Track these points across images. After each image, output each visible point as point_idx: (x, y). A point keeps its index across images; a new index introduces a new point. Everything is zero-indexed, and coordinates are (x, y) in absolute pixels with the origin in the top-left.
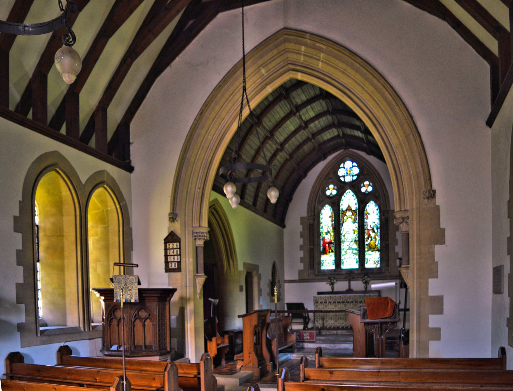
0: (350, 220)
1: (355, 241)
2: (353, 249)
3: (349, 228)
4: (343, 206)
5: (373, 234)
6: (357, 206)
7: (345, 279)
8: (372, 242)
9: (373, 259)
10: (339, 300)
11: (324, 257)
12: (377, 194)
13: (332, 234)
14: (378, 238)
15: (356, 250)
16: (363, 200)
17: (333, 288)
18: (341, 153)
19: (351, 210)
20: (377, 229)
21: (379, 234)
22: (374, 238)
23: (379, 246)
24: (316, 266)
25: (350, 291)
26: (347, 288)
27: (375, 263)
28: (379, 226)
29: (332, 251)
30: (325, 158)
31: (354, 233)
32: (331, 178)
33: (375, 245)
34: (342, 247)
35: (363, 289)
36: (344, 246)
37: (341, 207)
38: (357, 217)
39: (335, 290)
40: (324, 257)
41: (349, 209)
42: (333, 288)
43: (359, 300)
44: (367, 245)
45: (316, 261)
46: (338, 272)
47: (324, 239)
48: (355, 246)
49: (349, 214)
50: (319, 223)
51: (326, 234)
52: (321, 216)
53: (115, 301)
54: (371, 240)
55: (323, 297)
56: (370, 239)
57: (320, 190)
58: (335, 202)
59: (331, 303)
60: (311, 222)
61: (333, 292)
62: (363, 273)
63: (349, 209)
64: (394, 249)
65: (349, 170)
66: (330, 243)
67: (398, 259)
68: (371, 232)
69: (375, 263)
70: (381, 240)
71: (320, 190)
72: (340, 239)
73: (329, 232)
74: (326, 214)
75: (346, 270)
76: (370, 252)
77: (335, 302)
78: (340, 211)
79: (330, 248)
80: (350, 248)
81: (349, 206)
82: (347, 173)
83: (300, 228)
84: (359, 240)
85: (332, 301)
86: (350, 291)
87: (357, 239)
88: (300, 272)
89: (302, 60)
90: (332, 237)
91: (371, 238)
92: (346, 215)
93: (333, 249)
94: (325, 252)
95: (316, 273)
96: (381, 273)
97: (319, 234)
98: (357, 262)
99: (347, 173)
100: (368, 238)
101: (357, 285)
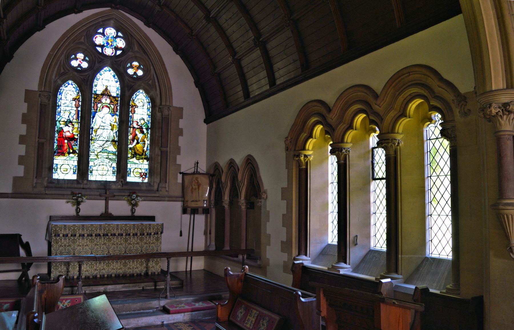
0: (106, 110)
1: (113, 141)
2: (109, 153)
3: (104, 121)
4: (99, 87)
5: (140, 136)
6: (119, 92)
7: (100, 197)
8: (137, 146)
9: (138, 170)
10: (98, 232)
11: (58, 160)
12: (150, 82)
13: (76, 125)
14: (147, 142)
15: (114, 154)
16: (129, 86)
17: (78, 210)
18: (97, 14)
19: (109, 96)
21: (149, 135)
22: (143, 141)
23: (148, 153)
24: (45, 173)
25: (106, 216)
26: (103, 210)
27: (141, 176)
28: (150, 125)
29: (74, 152)
30: (80, 11)
31: (112, 130)
32: (81, 43)
33: (143, 150)
34: (92, 148)
35: (129, 213)
36: (95, 146)
37: (94, 89)
38: (118, 108)
39: (137, 214)
40: (58, 160)
41: (106, 93)
42: (78, 210)
43: (132, 232)
44: (130, 148)
46: (81, 186)
47: (61, 131)
48: (112, 148)
49: (106, 101)
50: (55, 106)
52: (59, 97)
53: (430, 113)
54: (138, 143)
55: (70, 227)
56: (136, 141)
57: (63, 56)
58: (85, 81)
59: (84, 235)
61: (133, 218)
62: (121, 188)
63: (106, 93)
64: (175, 160)
65: (109, 40)
66: (72, 138)
67: (180, 173)
68: (137, 132)
69: (141, 176)
71: (63, 56)
72: (89, 134)
73: (71, 122)
74: (68, 94)
75: (96, 182)
76: (134, 160)
77: (91, 235)
78: (92, 94)
79: (70, 147)
80: (103, 151)
81: (106, 89)
82: (108, 43)
83: (24, 108)
85: (86, 233)
86: (106, 216)
87: (116, 139)
88: (16, 180)
90: (75, 130)
91: (138, 141)
92: (100, 102)
93: (76, 148)
96: (149, 191)
97: (54, 122)
98: (113, 173)
99: (108, 43)
101: (119, 207)
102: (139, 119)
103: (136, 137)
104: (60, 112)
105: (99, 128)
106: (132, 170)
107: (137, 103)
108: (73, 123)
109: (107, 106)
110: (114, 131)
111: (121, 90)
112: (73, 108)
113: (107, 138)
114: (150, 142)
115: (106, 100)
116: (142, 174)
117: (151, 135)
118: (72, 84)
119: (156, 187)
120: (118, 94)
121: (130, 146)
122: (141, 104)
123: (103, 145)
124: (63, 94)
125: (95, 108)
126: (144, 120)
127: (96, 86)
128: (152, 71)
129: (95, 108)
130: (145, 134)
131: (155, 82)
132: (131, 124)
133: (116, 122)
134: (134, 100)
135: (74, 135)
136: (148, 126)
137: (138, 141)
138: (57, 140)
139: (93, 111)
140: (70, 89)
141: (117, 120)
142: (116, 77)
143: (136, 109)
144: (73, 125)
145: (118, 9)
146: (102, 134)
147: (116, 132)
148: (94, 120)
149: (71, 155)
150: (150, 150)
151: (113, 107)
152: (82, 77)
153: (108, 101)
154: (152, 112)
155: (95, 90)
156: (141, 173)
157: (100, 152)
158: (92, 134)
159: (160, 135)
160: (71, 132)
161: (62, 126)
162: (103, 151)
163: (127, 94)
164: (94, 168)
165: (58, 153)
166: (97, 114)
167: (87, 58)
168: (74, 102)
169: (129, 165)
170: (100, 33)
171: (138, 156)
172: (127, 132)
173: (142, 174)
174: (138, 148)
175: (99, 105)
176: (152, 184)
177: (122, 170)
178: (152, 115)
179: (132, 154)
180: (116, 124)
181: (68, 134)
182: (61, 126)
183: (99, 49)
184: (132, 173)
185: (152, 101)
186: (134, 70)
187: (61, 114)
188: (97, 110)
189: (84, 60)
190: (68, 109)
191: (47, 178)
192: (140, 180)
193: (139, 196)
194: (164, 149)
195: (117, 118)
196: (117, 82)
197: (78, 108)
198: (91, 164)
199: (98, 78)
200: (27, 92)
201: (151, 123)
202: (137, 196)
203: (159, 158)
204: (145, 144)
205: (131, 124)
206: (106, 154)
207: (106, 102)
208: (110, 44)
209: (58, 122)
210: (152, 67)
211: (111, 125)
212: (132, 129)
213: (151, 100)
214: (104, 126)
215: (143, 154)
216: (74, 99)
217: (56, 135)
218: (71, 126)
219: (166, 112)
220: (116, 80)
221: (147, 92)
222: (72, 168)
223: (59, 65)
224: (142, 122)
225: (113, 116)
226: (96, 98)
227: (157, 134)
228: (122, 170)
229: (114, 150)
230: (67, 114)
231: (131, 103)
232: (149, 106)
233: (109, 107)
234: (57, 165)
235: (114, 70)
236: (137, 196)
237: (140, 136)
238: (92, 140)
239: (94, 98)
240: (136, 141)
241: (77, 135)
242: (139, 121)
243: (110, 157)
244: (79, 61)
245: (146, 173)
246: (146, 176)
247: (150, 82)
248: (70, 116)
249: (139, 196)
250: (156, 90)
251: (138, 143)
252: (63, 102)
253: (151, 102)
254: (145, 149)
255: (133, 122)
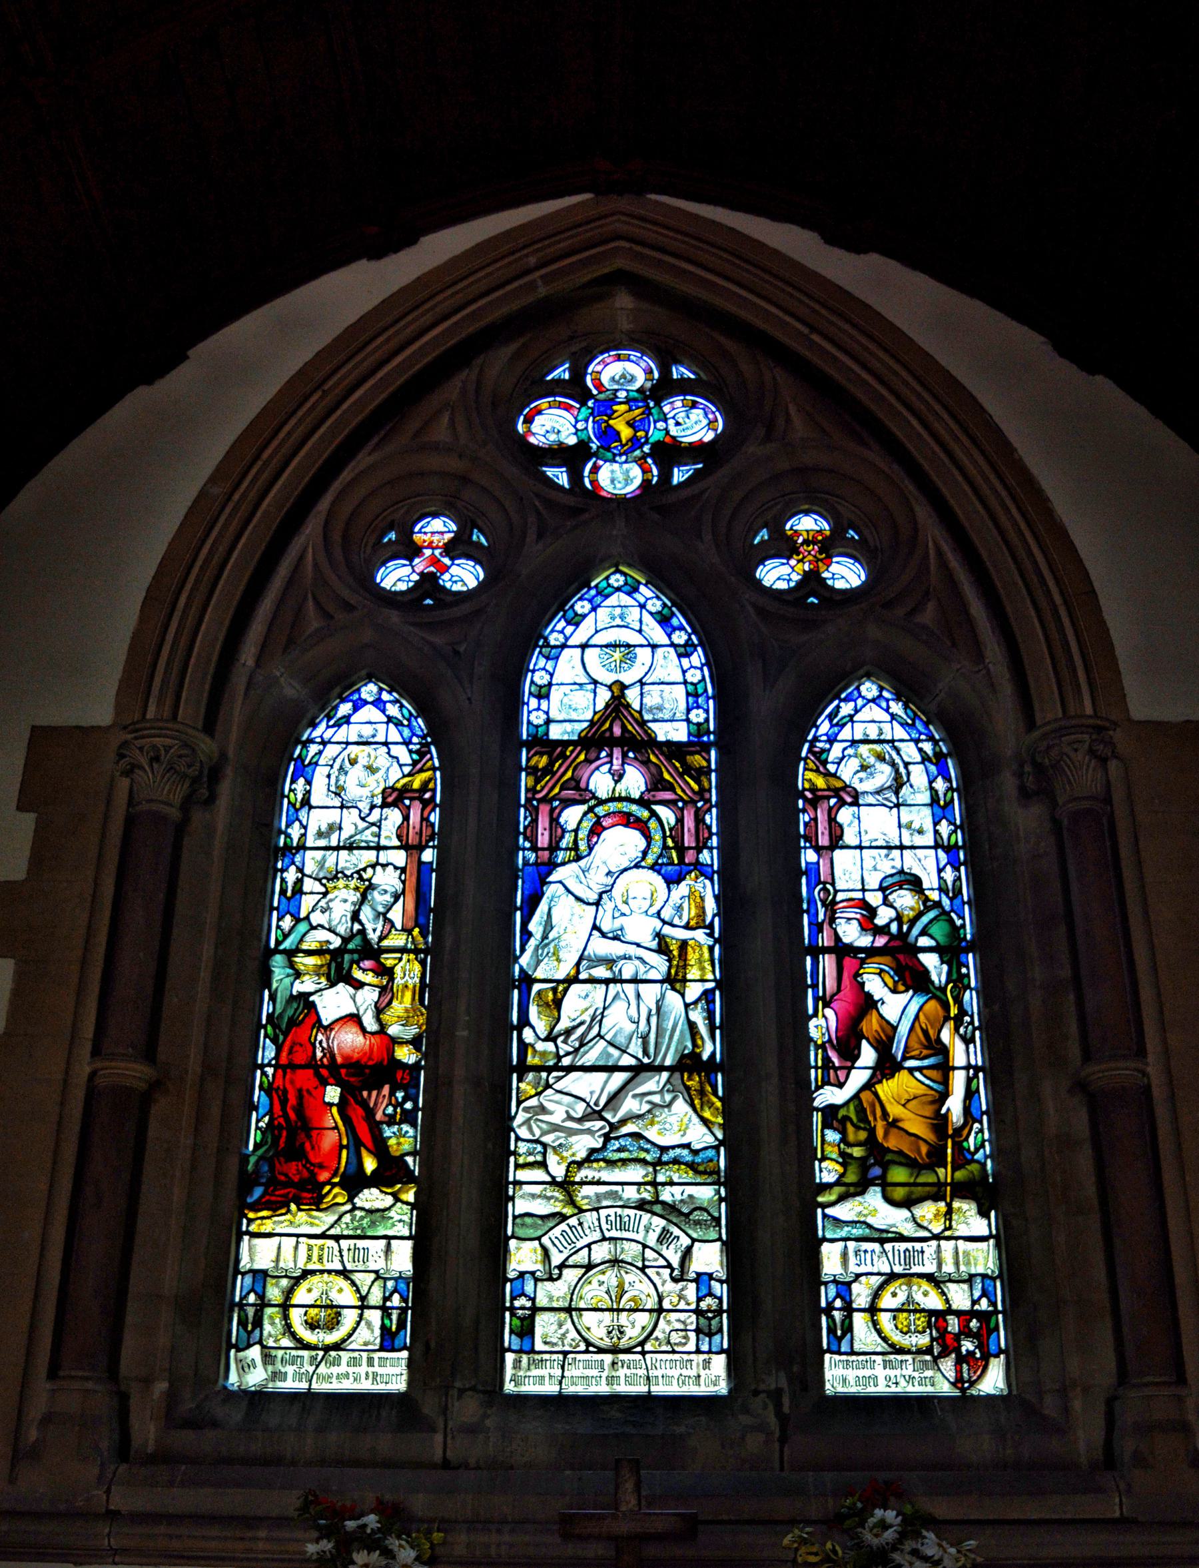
0: (620, 844)
1: (689, 1063)
3: (614, 916)
4: (565, 693)
5: (897, 1007)
8: (886, 1089)
13: (408, 972)
15: (699, 1169)
16: (771, 681)
20: (950, 952)
21: (971, 999)
22: (912, 1054)
23: (979, 1139)
27: (944, 1345)
29: (391, 1173)
33: (940, 1122)
36: (552, 1115)
37: (532, 714)
38: (712, 819)
41: (618, 730)
44: (830, 1112)
45: (162, 1269)
48: (684, 1126)
51: (337, 969)
54: (886, 1067)
56: (868, 1055)
58: (465, 681)
60: (163, 792)
66: (371, 1072)
69: (944, 1345)
70: (997, 1069)
72: (500, 1028)
73: (370, 952)
74: (358, 770)
76: (874, 1208)
81: (618, 704)
82: (608, 436)
84: (729, 1063)
89: (465, 1033)
92: (580, 793)
93: (403, 1139)
94: (293, 1180)
95: (146, 1431)
100: (847, 1046)
102: (873, 881)
103: (871, 1025)
104: (298, 890)
105: (572, 980)
106: (861, 1294)
107: (847, 772)
108: (389, 960)
109: (627, 820)
110: (694, 991)
111: (720, 697)
112: (384, 857)
113: (636, 1048)
114: (989, 1047)
115: (618, 777)
116: (953, 1324)
117: (984, 993)
118: (378, 703)
119: (1087, 1436)
120: (699, 730)
121: (829, 1096)
122: (884, 775)
123: (615, 1099)
124: (320, 774)
125: (543, 840)
126: (914, 883)
127: (543, 693)
128: (933, 533)
129: (543, 840)
130: (937, 994)
131: (964, 608)
132: (817, 927)
133: (700, 923)
134: (820, 758)
135: (394, 1041)
136: (955, 930)
137: (883, 1046)
138: (268, 1090)
139: (525, 856)
140: (367, 731)
141: (711, 906)
142: (678, 619)
143: (845, 815)
144: (389, 972)
145: (639, 188)
146: (598, 1018)
147: (707, 995)
148: (535, 926)
149: (371, 1198)
150: (995, 1112)
151: (667, 815)
152: (438, 640)
153: (635, 781)
154: (969, 826)
155: (538, 718)
156: (936, 1318)
157: (592, 1157)
158: (525, 1021)
159: (1066, 973)
160: (370, 1024)
161: (306, 985)
162: (616, 1140)
163: (765, 702)
164: (547, 1293)
165: (272, 1183)
166: (557, 875)
167: (478, 537)
168: (394, 816)
169: (831, 1260)
170: (557, 388)
171: (899, 1174)
172: (793, 986)
173: (953, 1324)
174: (894, 1110)
175: (571, 816)
176: (1050, 1405)
177: (773, 1298)
178: (971, 845)
179: (846, 1160)
180: (700, 935)
181: (349, 1040)
182: (298, 987)
183: (561, 477)
184: (859, 1320)
185: (962, 743)
186: (808, 559)
187: (307, 902)
188: (554, 847)
189: (457, 548)
190: (347, 861)
191: (161, 1386)
192: (940, 1381)
193: (931, 1522)
194: (1112, 1072)
195: (708, 891)
196: (684, 652)
197: (421, 848)
198: (522, 1257)
199: (555, 639)
200: (43, 740)
201: (977, 903)
202: (913, 1526)
203: (1084, 1161)
204: (945, 1069)
205: (817, 927)
206: (636, 1173)
207: (621, 789)
208: (626, 433)
209: (278, 960)
210: (923, 512)
211: (662, 948)
212: (828, 963)
213: (952, 735)
214: (610, 962)
215: (936, 1157)
216: (394, 797)
217: (268, 1052)
218: (369, 978)
219: (1082, 778)
220: (680, 638)
221: (908, 688)
222: (375, 1297)
223: (290, 582)
224: (905, 900)
225: (672, 881)
226: (548, 770)
227: (1037, 973)
228: (773, 1298)
229: (700, 1136)
230: (343, 899)
231: (807, 777)
232: (940, 785)
233: (641, 826)
234: (261, 1276)
235: (658, 581)
236: (913, 1526)
237: (897, 1007)
238: (523, 1069)
239: (532, 771)
240: (868, 1055)
241: (415, 1042)
242: (875, 899)
243: (666, 1195)
244: (437, 559)
245: (983, 1317)
246: (981, 1338)
247: (928, 615)
248: (366, 914)
249: (931, 1522)
250: (978, 655)
251: (886, 1067)
252: (317, 820)
253: (958, 752)
254: (954, 1105)
255: (831, 907)
